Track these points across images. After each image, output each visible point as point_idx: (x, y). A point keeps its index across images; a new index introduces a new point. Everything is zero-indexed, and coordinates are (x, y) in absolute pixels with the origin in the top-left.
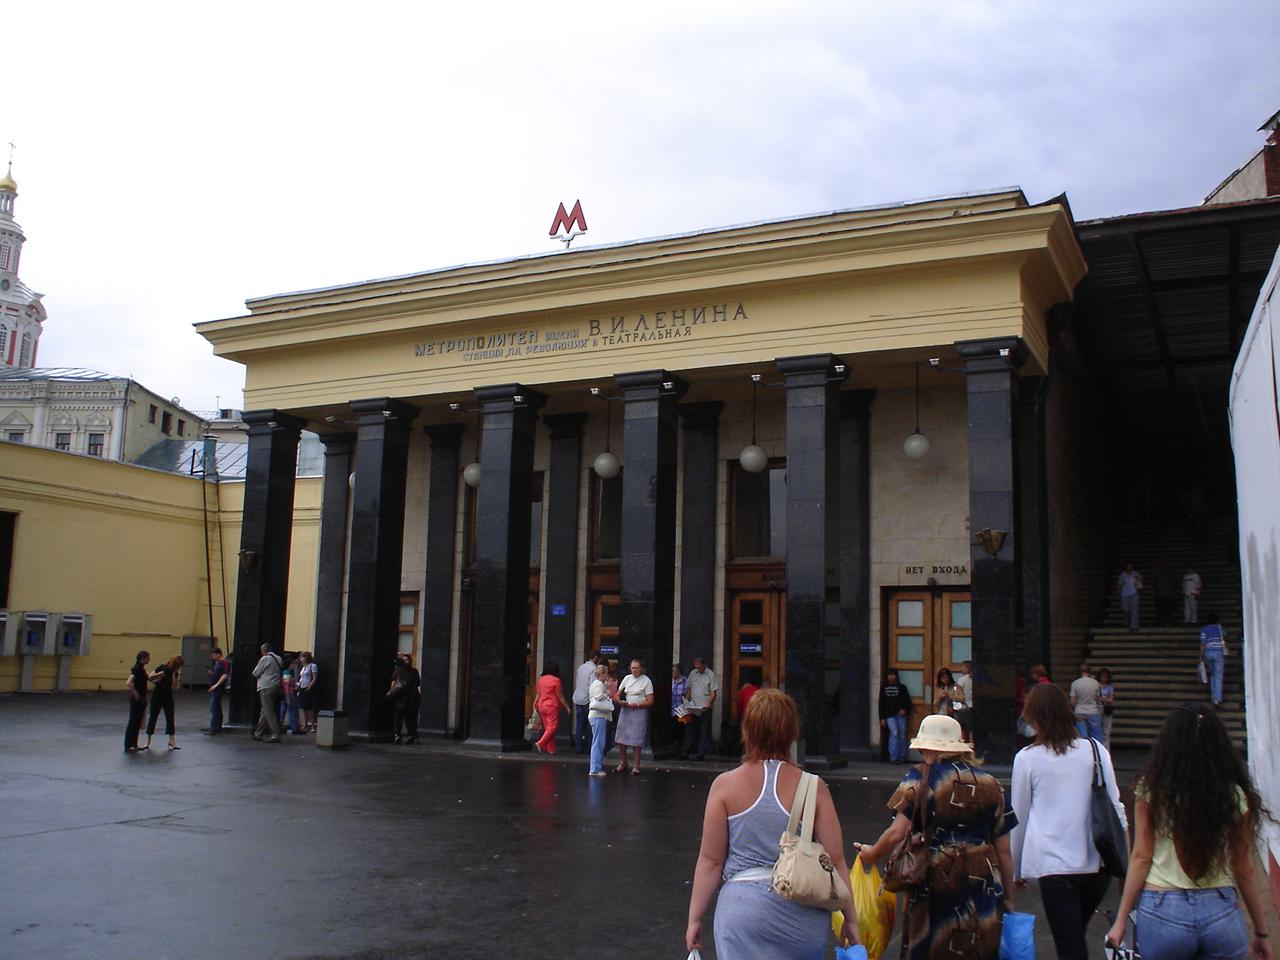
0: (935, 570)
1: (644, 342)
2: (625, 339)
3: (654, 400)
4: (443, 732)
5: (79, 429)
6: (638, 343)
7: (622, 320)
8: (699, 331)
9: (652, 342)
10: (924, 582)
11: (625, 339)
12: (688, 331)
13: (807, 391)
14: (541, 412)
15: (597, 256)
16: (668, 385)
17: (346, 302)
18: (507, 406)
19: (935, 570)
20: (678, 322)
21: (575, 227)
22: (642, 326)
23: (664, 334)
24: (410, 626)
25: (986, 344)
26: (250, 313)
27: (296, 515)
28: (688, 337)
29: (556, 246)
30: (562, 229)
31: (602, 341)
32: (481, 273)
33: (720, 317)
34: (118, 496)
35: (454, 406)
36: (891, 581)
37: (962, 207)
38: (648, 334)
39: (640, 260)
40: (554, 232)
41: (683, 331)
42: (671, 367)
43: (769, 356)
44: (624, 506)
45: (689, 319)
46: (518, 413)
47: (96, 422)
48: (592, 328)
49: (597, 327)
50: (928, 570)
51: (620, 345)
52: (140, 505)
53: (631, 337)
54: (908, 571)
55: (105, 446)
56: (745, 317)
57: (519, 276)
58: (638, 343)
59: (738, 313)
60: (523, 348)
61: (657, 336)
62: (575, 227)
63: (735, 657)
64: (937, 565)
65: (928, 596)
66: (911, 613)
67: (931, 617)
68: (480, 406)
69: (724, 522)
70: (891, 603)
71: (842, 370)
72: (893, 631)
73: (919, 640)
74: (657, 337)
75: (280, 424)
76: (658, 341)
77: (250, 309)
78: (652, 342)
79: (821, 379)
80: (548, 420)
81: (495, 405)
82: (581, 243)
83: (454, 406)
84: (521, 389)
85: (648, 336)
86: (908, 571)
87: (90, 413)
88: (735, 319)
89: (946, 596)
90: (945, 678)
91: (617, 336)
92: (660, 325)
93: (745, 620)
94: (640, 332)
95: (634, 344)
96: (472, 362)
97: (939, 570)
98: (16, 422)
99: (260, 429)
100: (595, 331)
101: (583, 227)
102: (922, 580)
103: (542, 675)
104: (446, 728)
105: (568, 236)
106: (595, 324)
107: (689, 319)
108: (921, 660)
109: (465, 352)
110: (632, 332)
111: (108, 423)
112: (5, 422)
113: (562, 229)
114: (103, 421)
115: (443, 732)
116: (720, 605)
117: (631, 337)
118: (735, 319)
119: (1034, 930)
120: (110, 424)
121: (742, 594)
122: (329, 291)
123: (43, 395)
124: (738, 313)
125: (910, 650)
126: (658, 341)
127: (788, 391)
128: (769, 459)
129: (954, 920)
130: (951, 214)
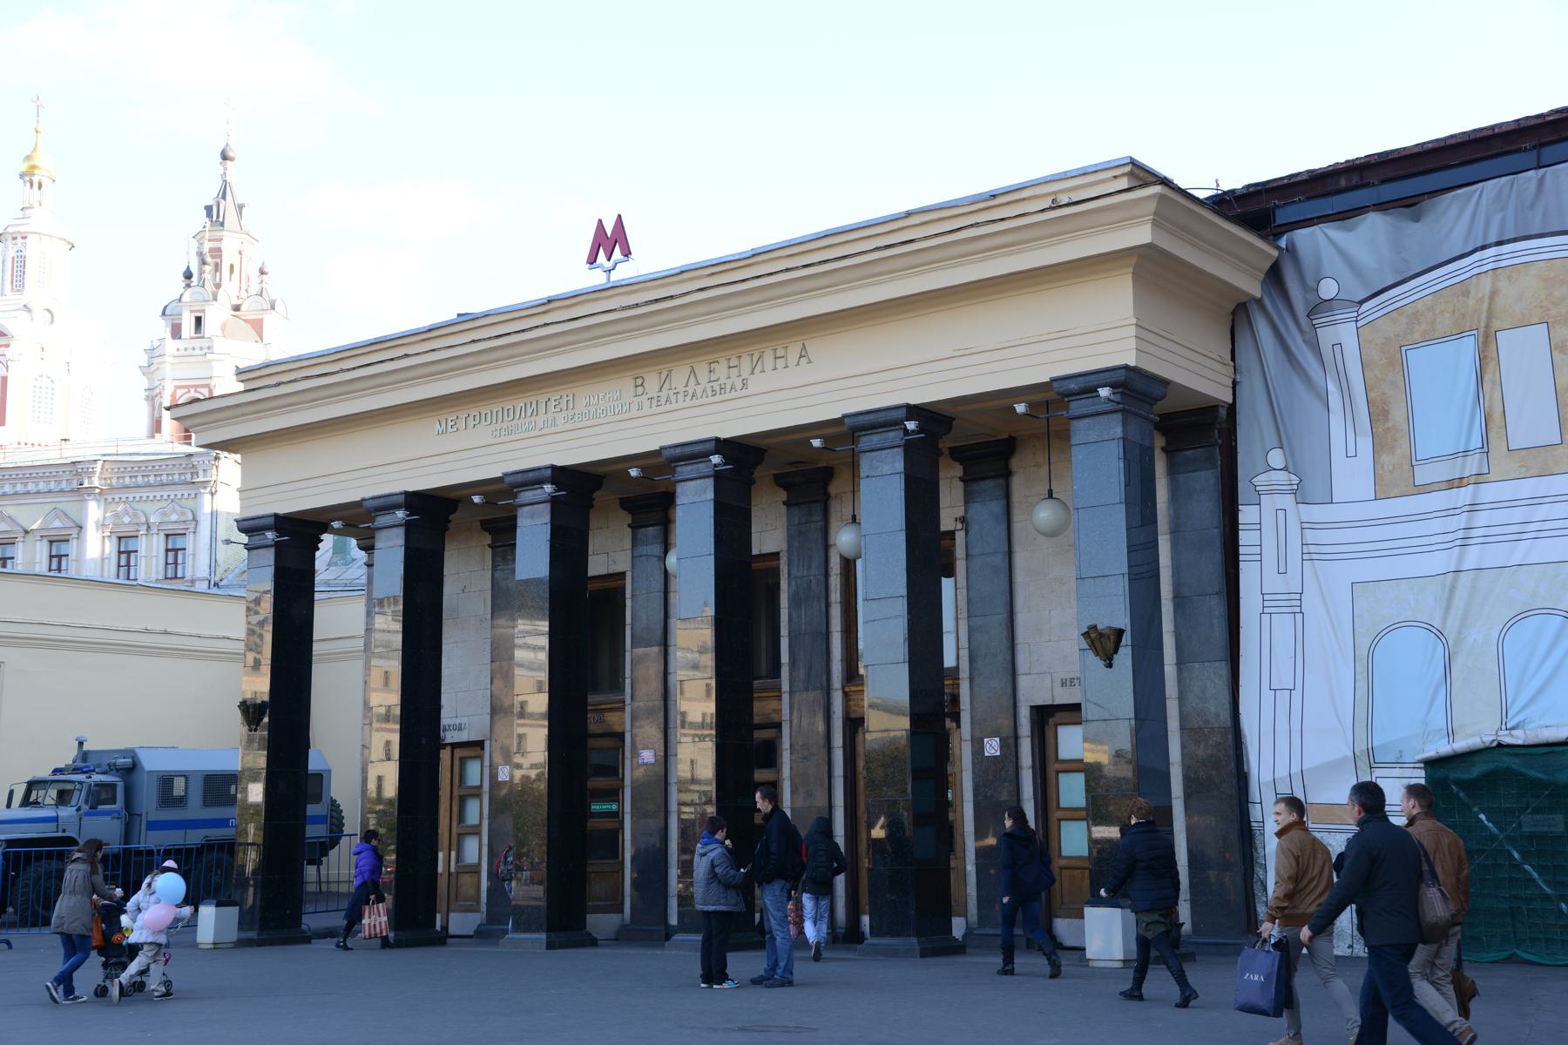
1: (695, 402)
3: (899, 446)
5: (149, 527)
9: (705, 401)
11: (673, 398)
12: (745, 385)
13: (1086, 421)
14: (945, 443)
17: (407, 356)
18: (894, 436)
21: (617, 254)
23: (718, 389)
24: (476, 787)
26: (241, 387)
27: (316, 648)
28: (744, 393)
29: (596, 278)
31: (647, 404)
34: (147, 631)
35: (816, 443)
36: (1043, 699)
38: (699, 390)
40: (592, 260)
42: (916, 399)
46: (911, 449)
48: (636, 386)
51: (669, 407)
53: (681, 396)
54: (1063, 684)
55: (189, 551)
60: (560, 418)
61: (710, 393)
68: (854, 441)
69: (839, 629)
70: (1047, 728)
72: (1052, 767)
75: (559, 488)
77: (242, 381)
78: (705, 401)
80: (957, 454)
81: (876, 438)
82: (625, 271)
84: (913, 411)
85: (699, 393)
86: (1063, 684)
87: (163, 504)
91: (664, 394)
92: (713, 379)
99: (257, 540)
100: (640, 390)
101: (627, 253)
103: (1464, 1012)
105: (609, 265)
106: (639, 381)
109: (492, 427)
110: (681, 389)
111: (190, 517)
114: (183, 514)
117: (681, 396)
118: (798, 364)
120: (194, 519)
126: (711, 399)
127: (861, 455)
129: (44, 791)
130: (1047, 203)
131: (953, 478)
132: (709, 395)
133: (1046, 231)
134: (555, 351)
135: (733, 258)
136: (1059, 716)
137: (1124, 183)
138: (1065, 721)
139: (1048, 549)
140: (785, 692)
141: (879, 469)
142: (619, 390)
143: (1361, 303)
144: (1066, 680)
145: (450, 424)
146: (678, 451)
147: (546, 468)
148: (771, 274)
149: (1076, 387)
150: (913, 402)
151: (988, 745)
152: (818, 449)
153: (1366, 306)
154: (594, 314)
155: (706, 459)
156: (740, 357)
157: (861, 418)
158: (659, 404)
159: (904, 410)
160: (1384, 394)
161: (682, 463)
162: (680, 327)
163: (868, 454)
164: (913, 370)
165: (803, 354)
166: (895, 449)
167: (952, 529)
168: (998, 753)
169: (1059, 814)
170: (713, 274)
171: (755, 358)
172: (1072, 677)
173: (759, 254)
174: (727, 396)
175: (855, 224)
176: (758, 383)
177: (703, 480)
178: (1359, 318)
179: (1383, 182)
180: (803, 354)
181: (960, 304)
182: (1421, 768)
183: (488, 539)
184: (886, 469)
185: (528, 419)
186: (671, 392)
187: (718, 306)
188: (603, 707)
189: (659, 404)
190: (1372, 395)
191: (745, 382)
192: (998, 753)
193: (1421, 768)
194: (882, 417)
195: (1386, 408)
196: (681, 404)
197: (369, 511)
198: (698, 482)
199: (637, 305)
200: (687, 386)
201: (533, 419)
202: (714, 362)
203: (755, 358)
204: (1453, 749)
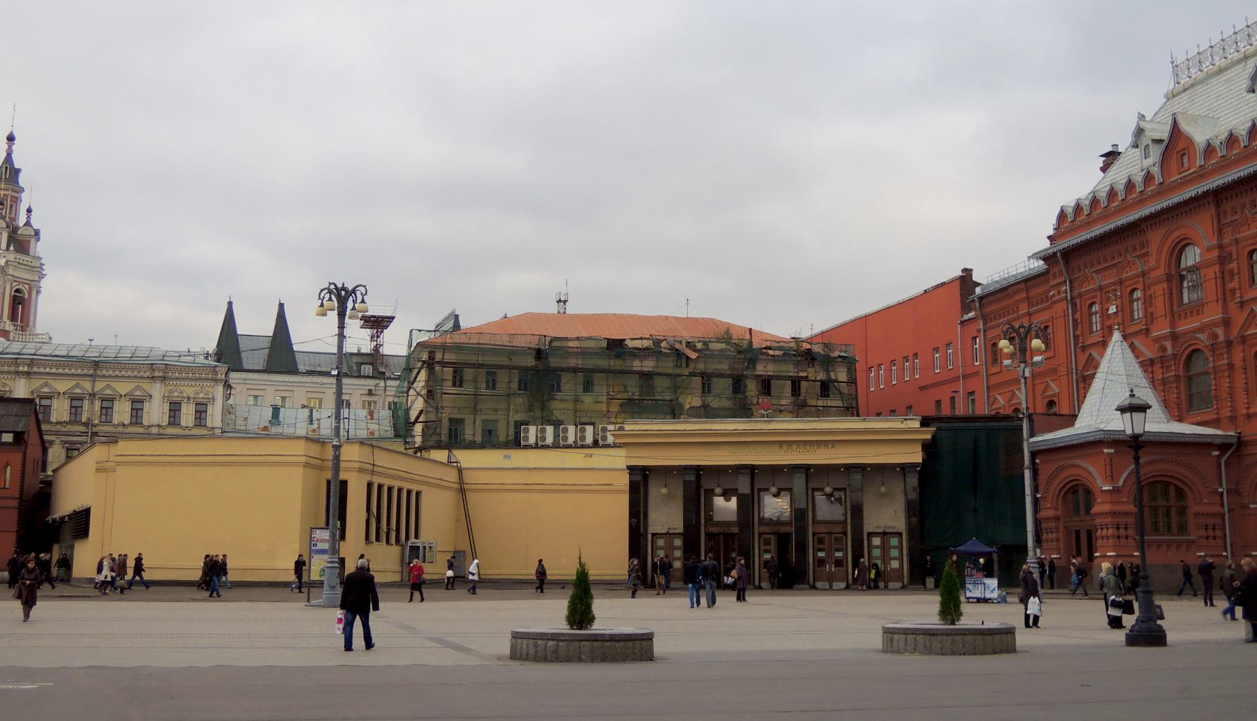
7: (791, 445)
8: (818, 451)
10: (881, 531)
12: (815, 451)
36: (871, 531)
44: (26, 397)
45: (815, 448)
47: (202, 395)
52: (413, 476)
56: (1212, 605)
65: (882, 535)
66: (877, 541)
67: (883, 542)
72: (655, 548)
90: (1084, 543)
91: (789, 450)
93: (765, 544)
94: (798, 450)
98: (138, 393)
107: (815, 448)
112: (130, 394)
116: (811, 539)
119: (940, 611)
123: (161, 374)
125: (876, 552)
136: (657, 536)
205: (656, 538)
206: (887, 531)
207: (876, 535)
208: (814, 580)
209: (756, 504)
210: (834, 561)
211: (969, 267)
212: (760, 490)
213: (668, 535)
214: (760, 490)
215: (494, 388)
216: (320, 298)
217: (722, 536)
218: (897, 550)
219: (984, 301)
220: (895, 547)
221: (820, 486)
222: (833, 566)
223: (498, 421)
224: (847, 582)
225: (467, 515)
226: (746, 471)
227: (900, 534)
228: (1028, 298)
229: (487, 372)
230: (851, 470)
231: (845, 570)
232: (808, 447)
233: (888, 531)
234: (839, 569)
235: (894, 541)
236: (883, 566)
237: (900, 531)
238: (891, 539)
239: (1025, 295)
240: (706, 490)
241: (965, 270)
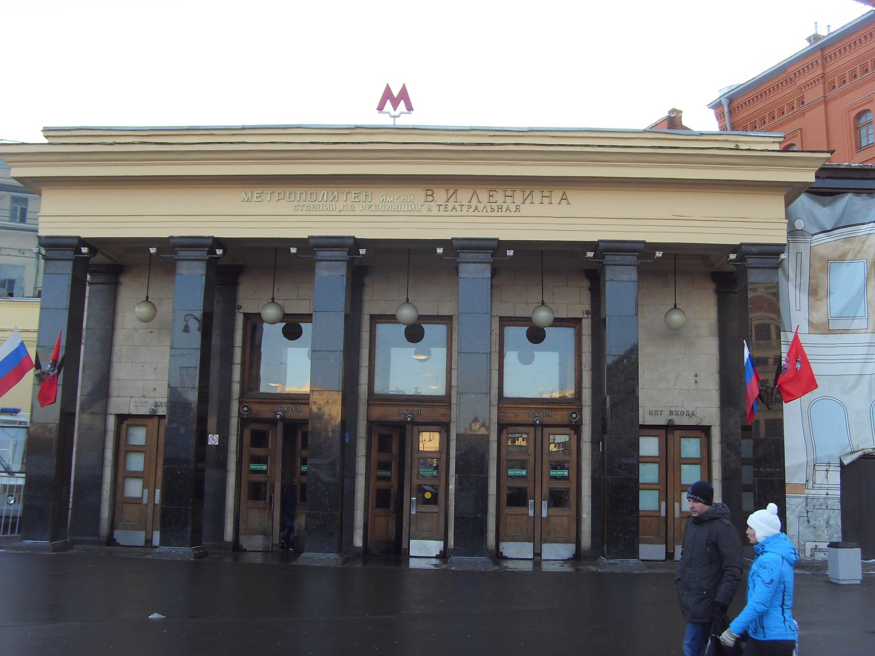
0: (671, 413)
1: (476, 213)
2: (459, 208)
4: (96, 539)
6: (471, 213)
11: (459, 208)
12: (517, 209)
13: (757, 270)
15: (380, 134)
16: (85, 250)
19: (671, 413)
20: (509, 200)
21: (402, 105)
22: (474, 200)
25: (759, 247)
26: (46, 141)
28: (517, 214)
30: (388, 105)
32: (314, 134)
33: (546, 200)
35: (153, 250)
37: (741, 142)
39: (492, 144)
40: (381, 108)
41: (513, 207)
43: (303, 234)
49: (431, 195)
50: (666, 413)
51: (454, 213)
53: (465, 208)
57: (94, 144)
58: (471, 213)
59: (562, 199)
61: (489, 209)
62: (402, 105)
63: (244, 473)
64: (673, 409)
65: (663, 432)
71: (661, 255)
72: (123, 448)
73: (656, 466)
74: (489, 211)
76: (489, 214)
79: (70, 254)
82: (406, 120)
83: (293, 250)
88: (560, 203)
89: (677, 433)
95: (468, 214)
96: (304, 213)
97: (675, 413)
100: (429, 199)
101: (410, 108)
102: (662, 421)
104: (97, 533)
106: (430, 193)
108: (657, 482)
109: (296, 203)
110: (465, 202)
113: (388, 105)
115: (96, 539)
117: (465, 208)
118: (560, 203)
121: (510, 428)
122: (505, 131)
124: (562, 199)
126: (489, 214)
127: (316, 262)
128: (555, 318)
130: (733, 146)
131: (582, 287)
132: (489, 211)
133: (759, 162)
134: (379, 161)
135: (513, 129)
136: (129, 421)
137: (777, 147)
138: (646, 434)
139: (643, 336)
140: (453, 404)
141: (619, 277)
142: (416, 196)
143: (813, 235)
144: (652, 411)
145: (396, 198)
146: (466, 243)
147: (209, 238)
148: (359, 143)
149: (756, 251)
150: (83, 236)
151: (211, 439)
152: (294, 254)
153: (815, 237)
154: (382, 143)
155: (776, 257)
156: (515, 191)
157: (766, 248)
158: (446, 210)
159: (212, 239)
160: (818, 282)
161: (466, 251)
162: (486, 164)
163: (612, 266)
164: (197, 218)
165: (564, 198)
166: (631, 267)
167: (581, 317)
168: (217, 444)
169: (658, 487)
170: (233, 135)
171: (526, 194)
172: (656, 409)
173: (533, 131)
174: (504, 214)
175: (229, 126)
176: (526, 209)
177: (481, 265)
178: (812, 242)
179: (827, 178)
180: (564, 198)
181: (359, 186)
182: (838, 466)
183: (712, 286)
184: (625, 278)
185: (328, 203)
186: (457, 205)
187: (566, 157)
188: (301, 401)
189: (446, 210)
190: (812, 281)
191: (517, 207)
192: (217, 444)
193: (838, 466)
194: (627, 246)
195: (817, 289)
196: (464, 213)
197: (175, 246)
198: (478, 265)
199: (463, 144)
200: (470, 202)
201: (334, 203)
202: (493, 191)
203: (526, 194)
204: (107, 448)
205: (129, 426)
206: (677, 423)
207: (646, 431)
208: (498, 540)
209: (365, 353)
210: (546, 491)
211: (678, 108)
212: (376, 319)
213: (156, 420)
214: (376, 319)
215: (23, 220)
216: (185, 320)
217: (280, 427)
218: (655, 467)
219: (827, 52)
220: (691, 461)
221: (521, 312)
222: (545, 503)
223: (24, 267)
224: (578, 542)
225: (159, 427)
226: (337, 254)
227: (705, 430)
228: (823, 76)
229: (13, 197)
230: (608, 258)
231: (574, 513)
232: (499, 196)
233: (679, 421)
234: (557, 511)
235: (691, 447)
236: (663, 504)
237: (705, 423)
238: (684, 442)
239: (820, 71)
240: (247, 316)
241: (674, 111)
